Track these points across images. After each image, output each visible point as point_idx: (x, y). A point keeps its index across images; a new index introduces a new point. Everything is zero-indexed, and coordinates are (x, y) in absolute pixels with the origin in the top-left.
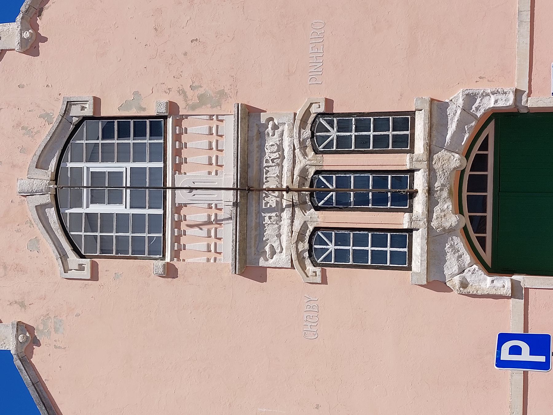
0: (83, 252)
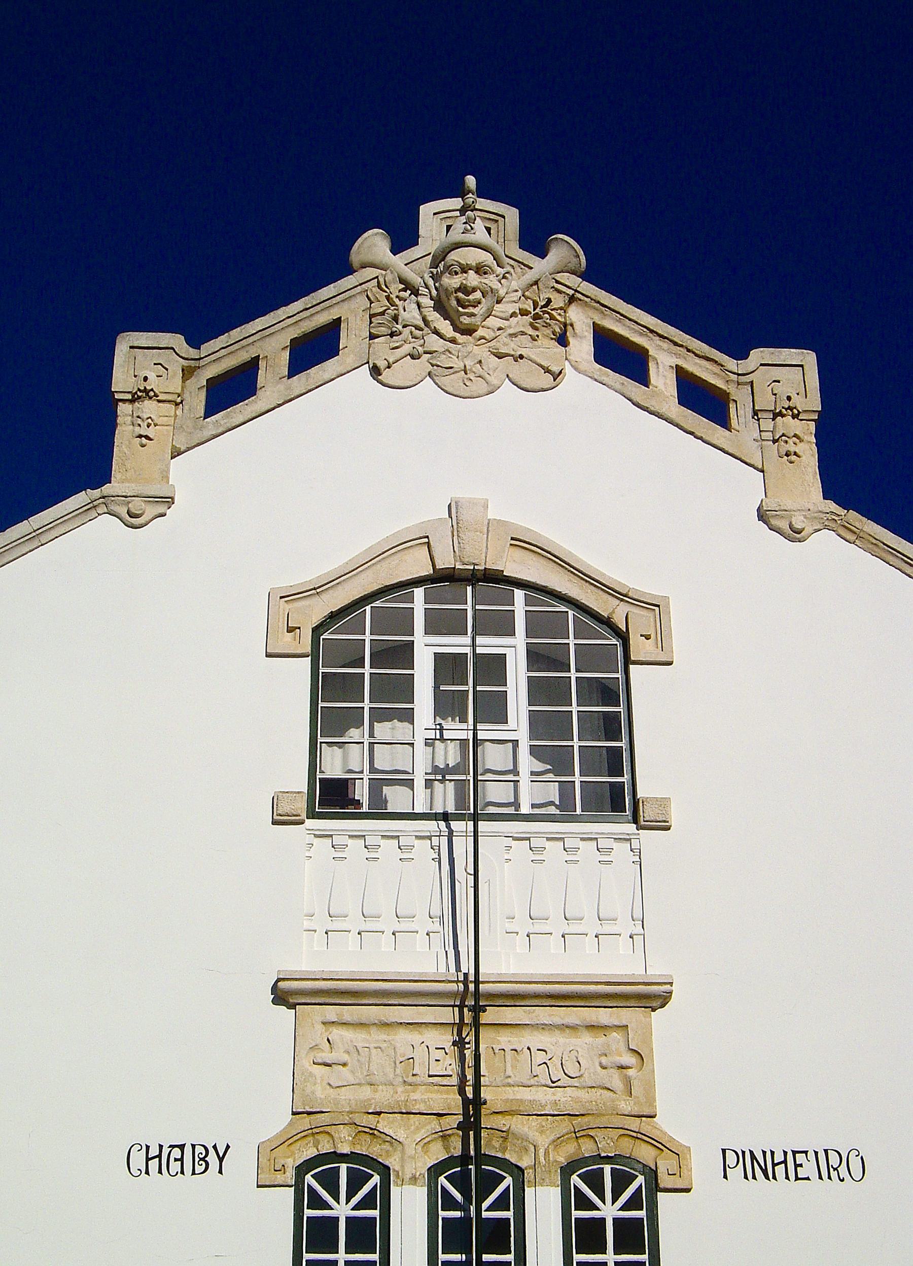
0: (326, 636)
